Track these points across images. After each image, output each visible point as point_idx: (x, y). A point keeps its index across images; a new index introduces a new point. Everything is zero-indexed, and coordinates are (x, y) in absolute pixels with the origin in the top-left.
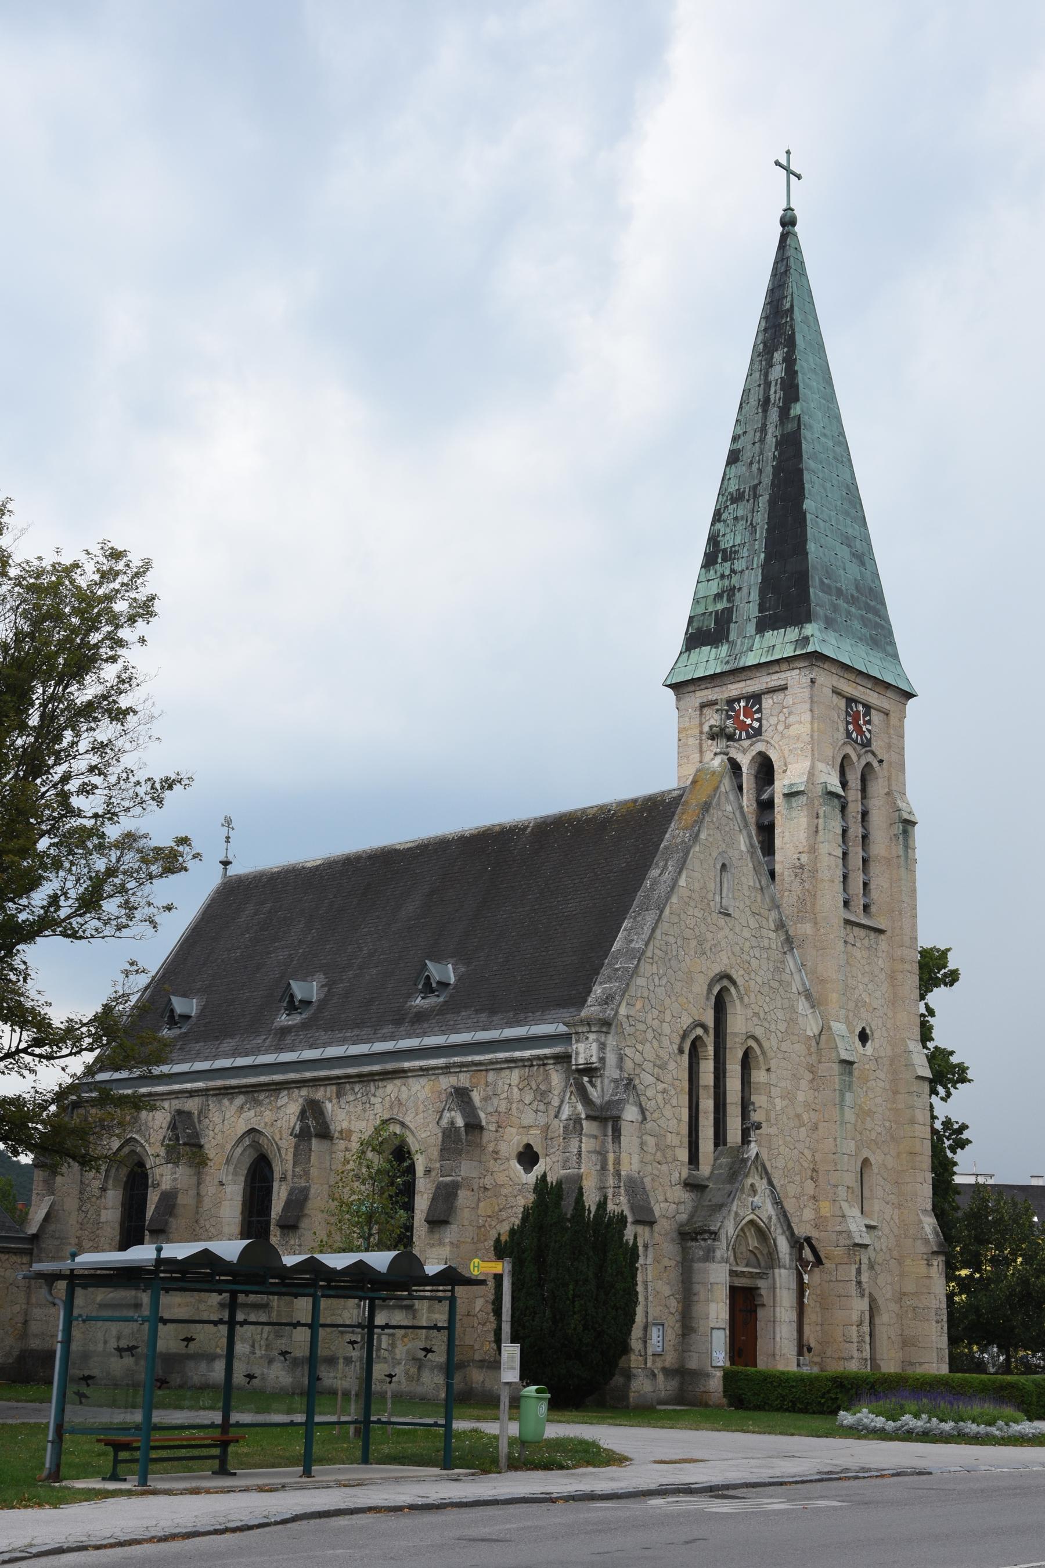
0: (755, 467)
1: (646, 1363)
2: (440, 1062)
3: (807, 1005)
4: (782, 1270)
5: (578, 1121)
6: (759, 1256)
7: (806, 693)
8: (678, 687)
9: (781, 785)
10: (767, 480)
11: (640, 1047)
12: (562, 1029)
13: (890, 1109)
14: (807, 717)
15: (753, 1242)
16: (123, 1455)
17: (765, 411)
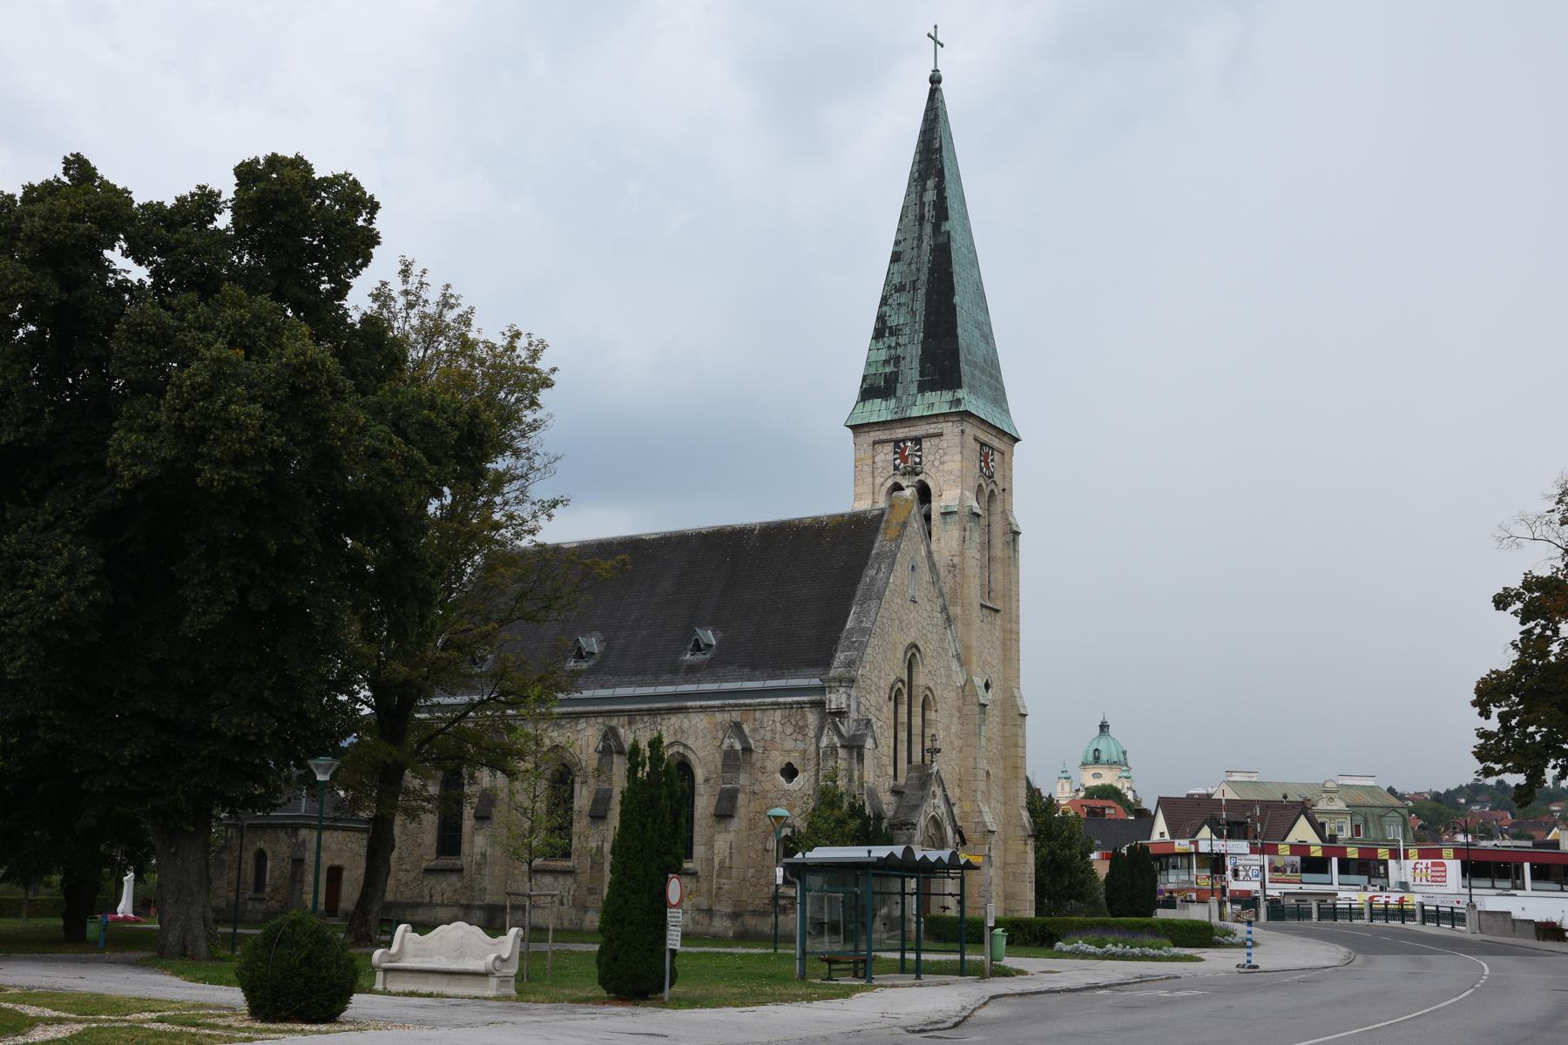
0: (914, 267)
2: (718, 703)
5: (834, 749)
7: (958, 440)
8: (856, 428)
9: (937, 506)
10: (924, 277)
12: (816, 682)
14: (958, 457)
15: (932, 831)
16: (834, 966)
17: (921, 224)
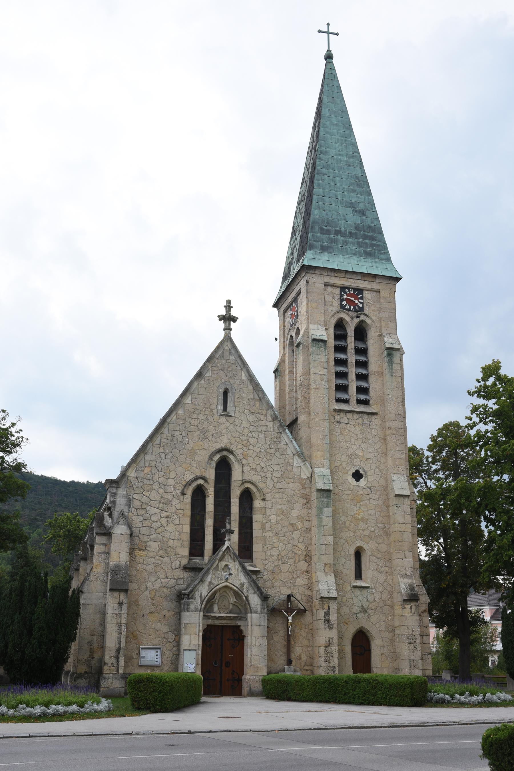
1: (118, 671)
3: (300, 461)
4: (254, 615)
6: (240, 607)
11: (147, 494)
13: (383, 517)
